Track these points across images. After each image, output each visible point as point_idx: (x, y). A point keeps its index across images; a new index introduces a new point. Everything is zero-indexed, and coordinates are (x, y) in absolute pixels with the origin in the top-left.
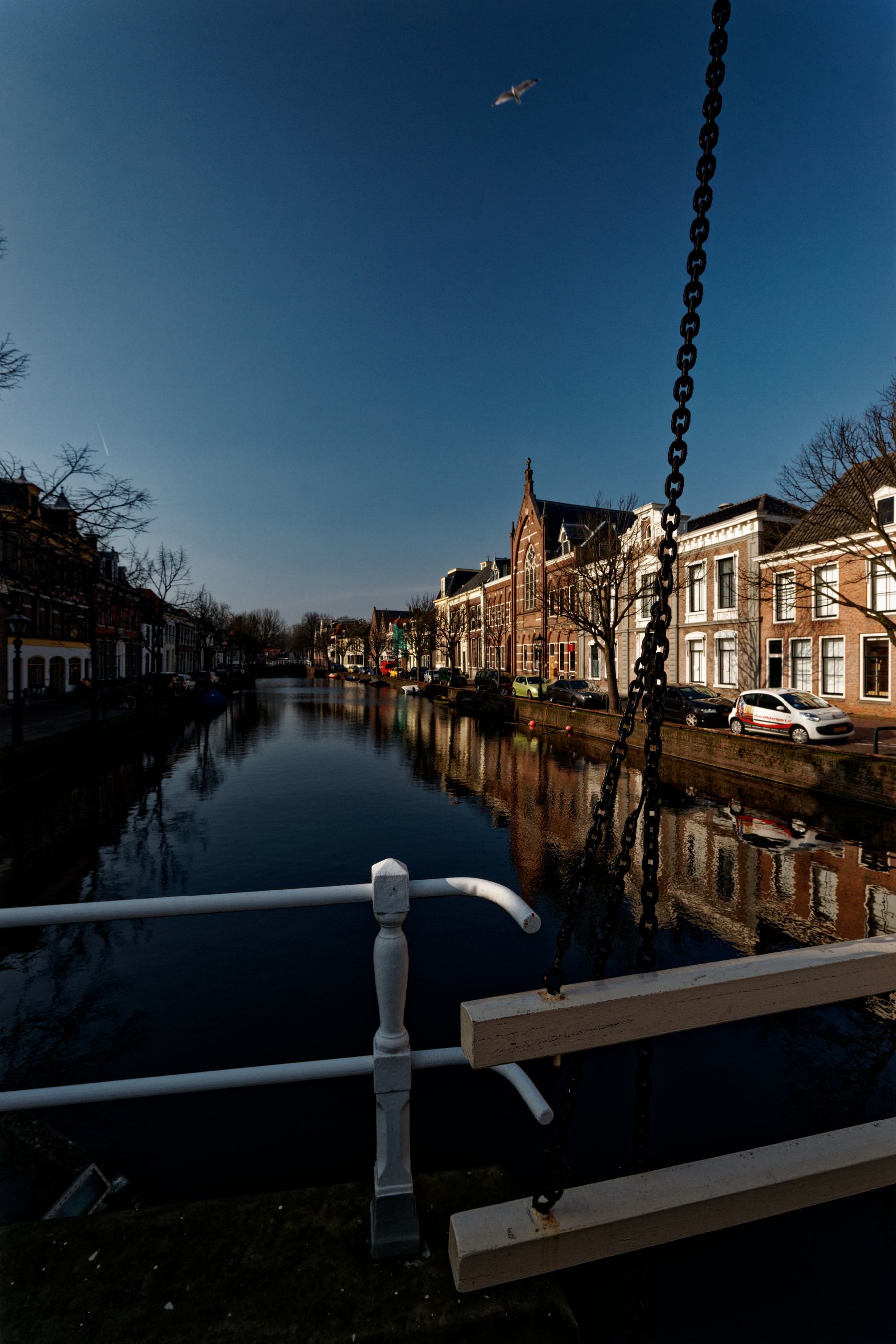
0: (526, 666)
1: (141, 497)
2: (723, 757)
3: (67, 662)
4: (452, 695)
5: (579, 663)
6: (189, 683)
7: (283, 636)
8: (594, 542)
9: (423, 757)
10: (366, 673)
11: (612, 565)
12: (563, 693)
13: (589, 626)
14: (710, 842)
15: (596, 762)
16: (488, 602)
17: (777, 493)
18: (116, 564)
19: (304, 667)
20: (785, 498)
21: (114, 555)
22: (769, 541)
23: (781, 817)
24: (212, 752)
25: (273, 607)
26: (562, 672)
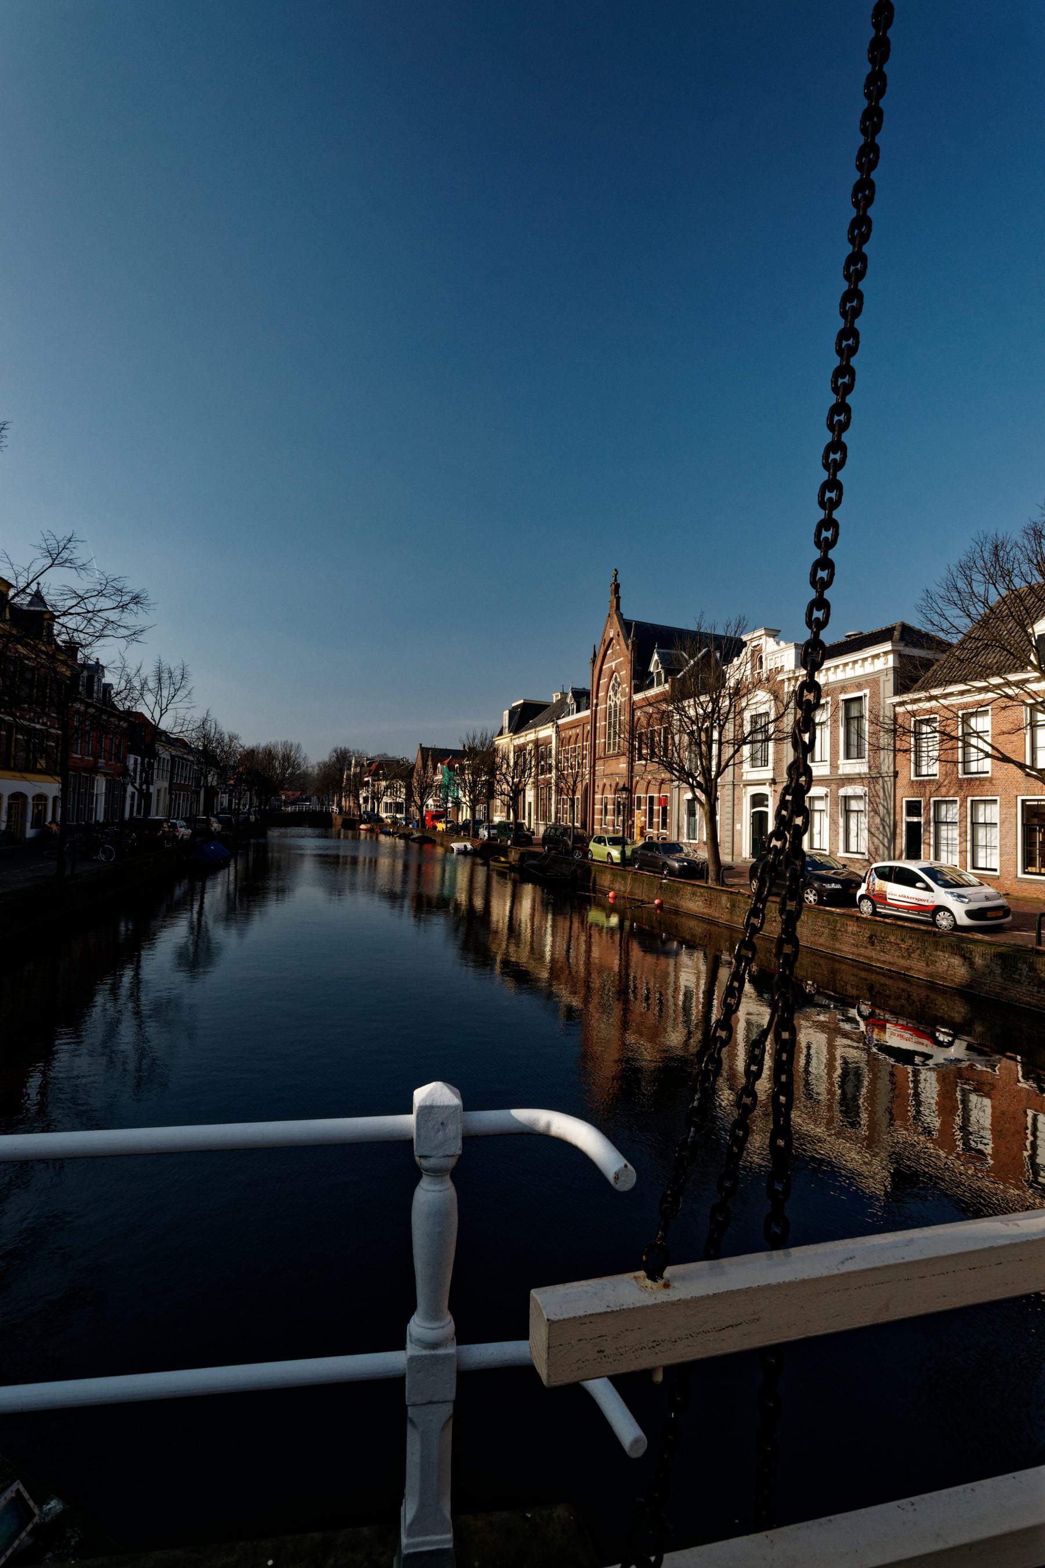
0: (606, 823)
1: (136, 599)
2: (850, 944)
3: (30, 800)
4: (514, 856)
5: (672, 820)
6: (184, 832)
7: (305, 775)
8: (693, 673)
9: (473, 929)
10: (407, 825)
11: (715, 701)
12: (652, 858)
13: (685, 776)
14: (831, 1047)
15: (692, 946)
16: (561, 741)
17: (916, 622)
18: (100, 680)
19: (329, 815)
20: (925, 628)
21: (98, 669)
22: (907, 678)
23: (924, 1023)
24: (209, 919)
25: (293, 739)
26: (652, 832)
